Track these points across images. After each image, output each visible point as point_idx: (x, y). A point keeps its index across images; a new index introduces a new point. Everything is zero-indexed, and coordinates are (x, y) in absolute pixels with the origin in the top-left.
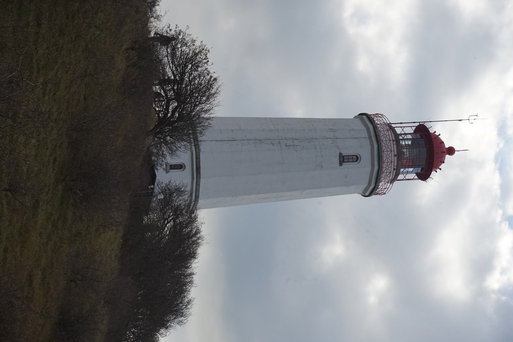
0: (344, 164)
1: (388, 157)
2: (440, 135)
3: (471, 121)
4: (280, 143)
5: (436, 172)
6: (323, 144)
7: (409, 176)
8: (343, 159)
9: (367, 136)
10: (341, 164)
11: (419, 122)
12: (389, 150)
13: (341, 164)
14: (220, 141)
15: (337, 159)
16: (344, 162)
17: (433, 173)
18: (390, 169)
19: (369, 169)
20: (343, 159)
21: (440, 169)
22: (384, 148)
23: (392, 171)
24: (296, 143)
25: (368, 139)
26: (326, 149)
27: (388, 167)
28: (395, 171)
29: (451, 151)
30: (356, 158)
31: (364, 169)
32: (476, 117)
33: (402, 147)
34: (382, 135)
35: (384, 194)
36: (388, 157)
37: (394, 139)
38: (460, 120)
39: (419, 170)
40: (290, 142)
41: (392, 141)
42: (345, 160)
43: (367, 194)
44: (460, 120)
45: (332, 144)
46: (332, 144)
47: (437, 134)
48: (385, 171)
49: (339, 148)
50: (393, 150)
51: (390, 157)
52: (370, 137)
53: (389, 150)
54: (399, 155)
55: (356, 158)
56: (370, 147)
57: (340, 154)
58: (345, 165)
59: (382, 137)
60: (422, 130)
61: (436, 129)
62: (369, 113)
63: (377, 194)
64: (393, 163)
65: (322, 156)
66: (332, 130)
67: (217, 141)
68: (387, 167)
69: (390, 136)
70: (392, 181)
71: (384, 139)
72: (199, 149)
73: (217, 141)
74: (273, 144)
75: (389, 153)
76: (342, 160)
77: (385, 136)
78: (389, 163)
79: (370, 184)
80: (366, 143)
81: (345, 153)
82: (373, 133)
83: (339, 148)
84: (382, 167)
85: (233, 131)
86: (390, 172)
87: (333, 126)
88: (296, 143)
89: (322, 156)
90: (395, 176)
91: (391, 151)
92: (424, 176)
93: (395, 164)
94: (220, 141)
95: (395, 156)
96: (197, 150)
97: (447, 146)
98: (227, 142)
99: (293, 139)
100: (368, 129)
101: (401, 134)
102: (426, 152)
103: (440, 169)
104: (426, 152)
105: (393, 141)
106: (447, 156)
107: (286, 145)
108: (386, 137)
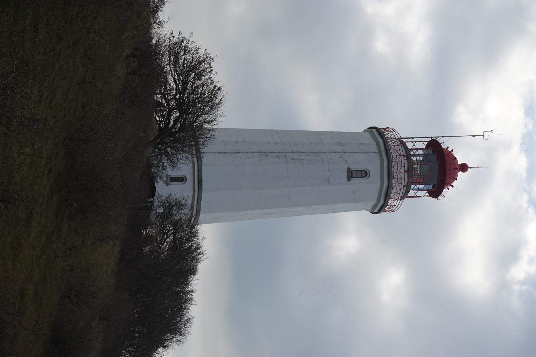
0: (352, 179)
2: (452, 151)
5: (448, 189)
6: (331, 158)
7: (420, 193)
8: (351, 174)
9: (377, 151)
10: (349, 180)
12: (399, 165)
13: (349, 180)
14: (224, 153)
15: (345, 175)
16: (352, 177)
17: (445, 190)
19: (379, 184)
20: (351, 174)
21: (453, 186)
22: (394, 163)
23: (402, 187)
24: (302, 156)
25: (378, 154)
26: (334, 163)
27: (399, 183)
28: (405, 188)
29: (464, 168)
30: (364, 174)
31: (372, 186)
32: (490, 133)
34: (392, 149)
35: (394, 211)
37: (405, 154)
40: (296, 156)
41: (402, 157)
43: (376, 211)
46: (340, 158)
47: (450, 149)
48: (395, 188)
50: (403, 165)
52: (380, 152)
53: (399, 165)
54: (410, 170)
55: (364, 174)
56: (380, 162)
57: (349, 169)
58: (353, 180)
59: (393, 152)
60: (434, 145)
62: (379, 126)
63: (386, 211)
64: (403, 179)
65: (329, 171)
66: (340, 144)
67: (220, 153)
69: (401, 151)
70: (402, 198)
72: (201, 161)
73: (220, 153)
75: (399, 168)
76: (350, 175)
77: (395, 151)
79: (379, 200)
80: (376, 157)
81: (353, 168)
84: (392, 183)
85: (237, 143)
86: (400, 189)
87: (340, 141)
88: (302, 156)
89: (329, 171)
93: (406, 181)
94: (224, 153)
95: (406, 171)
96: (199, 162)
97: (460, 162)
98: (230, 154)
99: (300, 153)
100: (378, 143)
101: (412, 150)
102: (438, 168)
103: (453, 186)
104: (438, 168)
105: (404, 156)
106: (460, 173)
107: (292, 159)
108: (396, 151)
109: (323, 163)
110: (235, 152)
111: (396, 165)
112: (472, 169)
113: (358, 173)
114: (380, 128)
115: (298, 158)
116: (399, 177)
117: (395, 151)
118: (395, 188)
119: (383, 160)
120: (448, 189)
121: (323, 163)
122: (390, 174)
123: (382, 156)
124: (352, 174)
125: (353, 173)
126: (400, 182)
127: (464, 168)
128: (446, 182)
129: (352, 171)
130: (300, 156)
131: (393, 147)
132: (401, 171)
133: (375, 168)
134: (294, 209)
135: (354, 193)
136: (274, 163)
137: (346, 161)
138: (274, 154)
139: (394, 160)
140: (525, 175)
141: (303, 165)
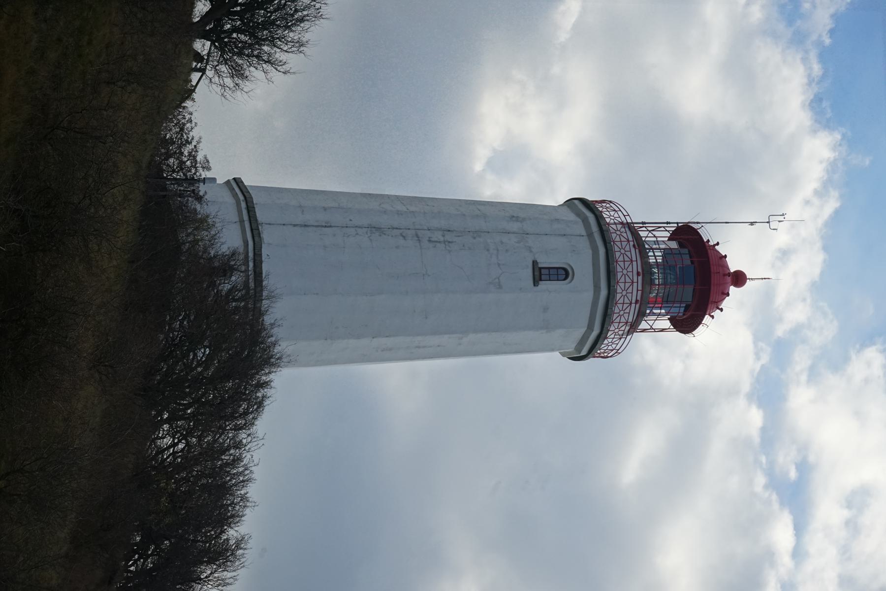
0: (541, 282)
1: (625, 272)
2: (718, 244)
3: (773, 225)
4: (417, 236)
6: (502, 243)
8: (540, 274)
9: (584, 233)
10: (536, 283)
11: (677, 223)
13: (536, 283)
14: (301, 226)
16: (541, 280)
17: (707, 319)
18: (629, 295)
19: (589, 296)
20: (540, 274)
22: (618, 254)
24: (448, 237)
25: (586, 238)
26: (507, 251)
27: (624, 312)
28: (640, 278)
29: (739, 279)
30: (563, 274)
31: (578, 297)
32: (781, 218)
33: (651, 266)
34: (612, 231)
36: (624, 293)
38: (752, 223)
39: (678, 310)
40: (438, 236)
42: (543, 277)
43: (584, 353)
44: (752, 223)
45: (518, 242)
49: (531, 251)
50: (634, 259)
51: (629, 288)
52: (590, 235)
54: (646, 271)
55: (563, 274)
56: (590, 252)
57: (535, 263)
58: (543, 285)
59: (614, 235)
60: (686, 235)
61: (710, 234)
62: (590, 198)
64: (635, 284)
65: (499, 265)
67: (295, 225)
68: (622, 313)
70: (633, 327)
71: (618, 239)
73: (295, 225)
74: (404, 237)
76: (537, 273)
78: (625, 306)
79: (590, 327)
82: (595, 228)
83: (531, 251)
84: (614, 252)
85: (325, 209)
86: (631, 303)
87: (521, 217)
88: (448, 237)
89: (499, 265)
90: (638, 316)
91: (632, 261)
92: (687, 323)
93: (640, 288)
94: (301, 226)
96: (256, 239)
97: (732, 269)
98: (315, 228)
100: (585, 221)
102: (693, 278)
104: (693, 278)
106: (732, 289)
107: (430, 241)
108: (621, 240)
109: (488, 250)
110: (324, 224)
111: (623, 280)
112: (752, 282)
113: (552, 271)
114: (590, 199)
115: (442, 239)
116: (626, 301)
117: (618, 233)
118: (621, 301)
119: (597, 247)
120: (713, 317)
121: (488, 250)
122: (612, 274)
123: (599, 279)
124: (541, 274)
125: (543, 271)
126: (627, 311)
127: (739, 279)
128: (711, 299)
129: (540, 269)
130: (443, 236)
131: (614, 226)
132: (630, 269)
133: (582, 261)
134: (434, 340)
135: (545, 309)
136: (397, 247)
137: (530, 249)
138: (397, 232)
139: (617, 249)
140: (757, 440)
141: (450, 251)
